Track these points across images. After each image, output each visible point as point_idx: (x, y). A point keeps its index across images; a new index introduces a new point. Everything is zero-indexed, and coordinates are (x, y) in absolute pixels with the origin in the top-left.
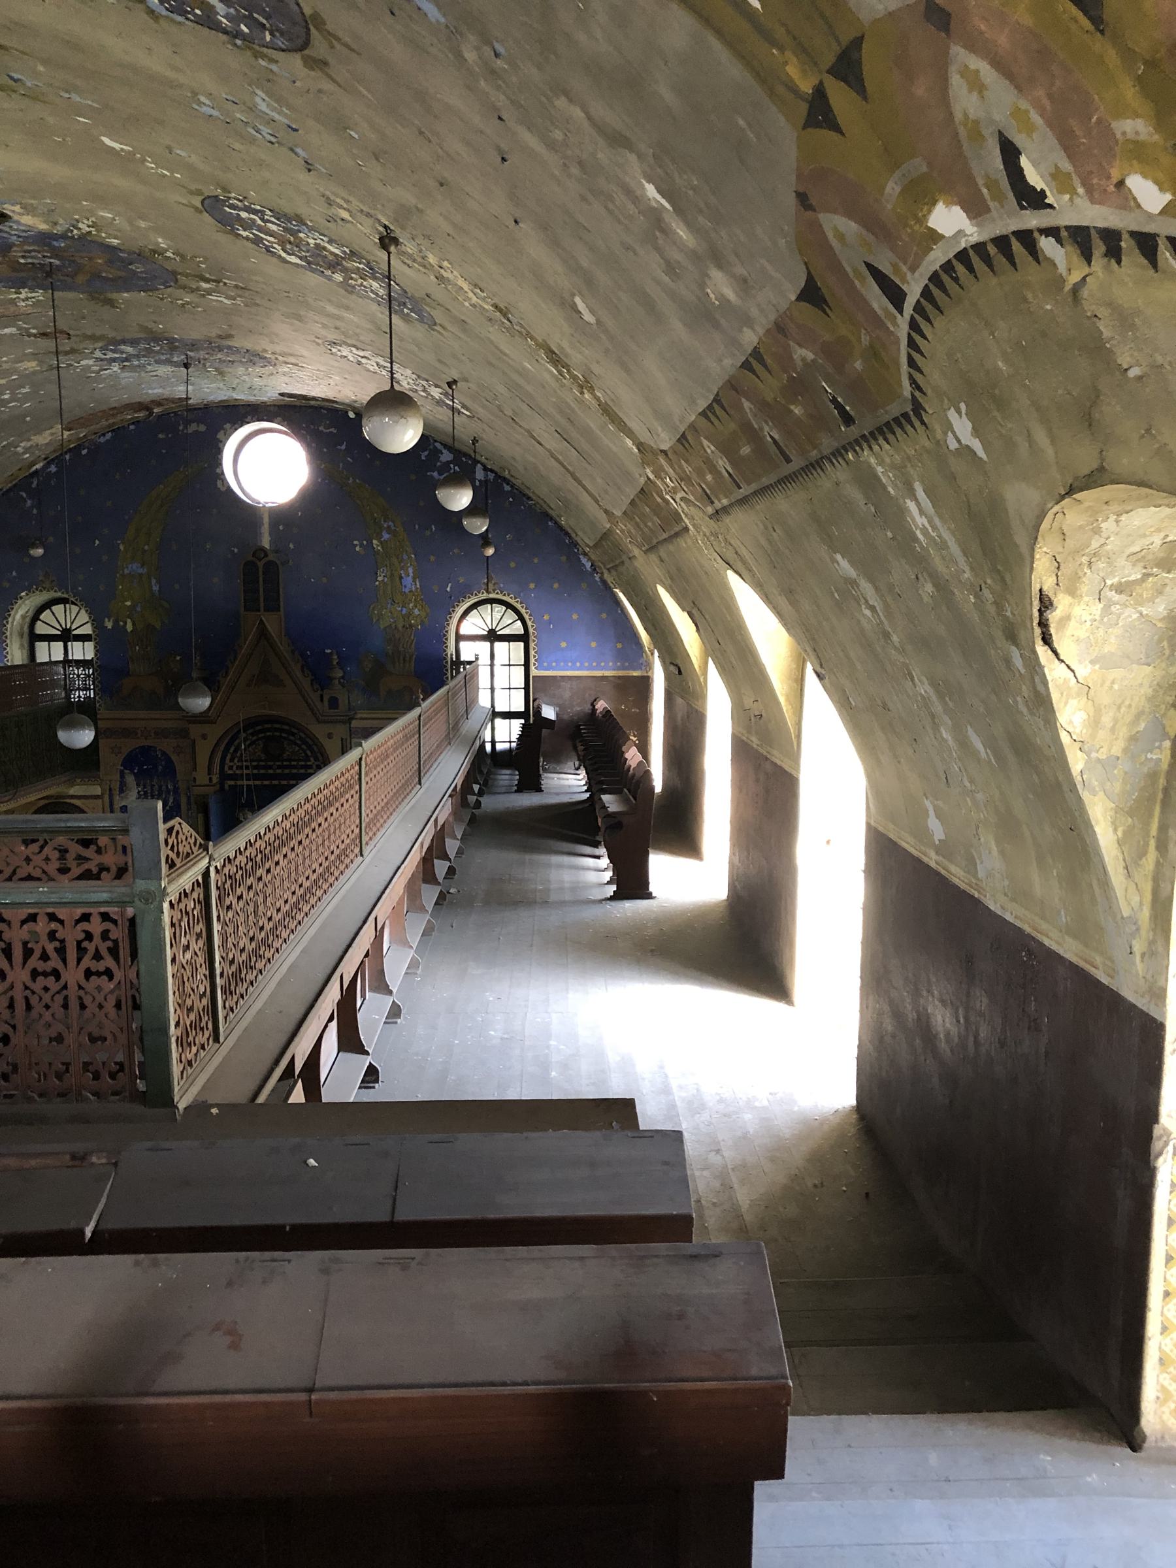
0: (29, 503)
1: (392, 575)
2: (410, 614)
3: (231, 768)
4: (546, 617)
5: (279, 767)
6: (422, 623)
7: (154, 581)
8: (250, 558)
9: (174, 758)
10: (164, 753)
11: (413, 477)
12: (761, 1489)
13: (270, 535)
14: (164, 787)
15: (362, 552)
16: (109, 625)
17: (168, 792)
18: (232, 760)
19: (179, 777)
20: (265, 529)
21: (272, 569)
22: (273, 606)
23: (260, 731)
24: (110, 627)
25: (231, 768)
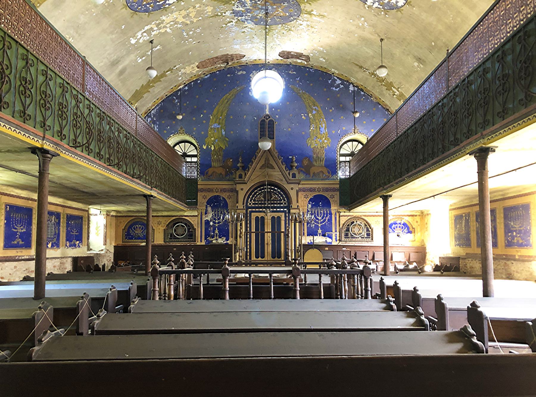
7: (223, 130)
10: (223, 198)
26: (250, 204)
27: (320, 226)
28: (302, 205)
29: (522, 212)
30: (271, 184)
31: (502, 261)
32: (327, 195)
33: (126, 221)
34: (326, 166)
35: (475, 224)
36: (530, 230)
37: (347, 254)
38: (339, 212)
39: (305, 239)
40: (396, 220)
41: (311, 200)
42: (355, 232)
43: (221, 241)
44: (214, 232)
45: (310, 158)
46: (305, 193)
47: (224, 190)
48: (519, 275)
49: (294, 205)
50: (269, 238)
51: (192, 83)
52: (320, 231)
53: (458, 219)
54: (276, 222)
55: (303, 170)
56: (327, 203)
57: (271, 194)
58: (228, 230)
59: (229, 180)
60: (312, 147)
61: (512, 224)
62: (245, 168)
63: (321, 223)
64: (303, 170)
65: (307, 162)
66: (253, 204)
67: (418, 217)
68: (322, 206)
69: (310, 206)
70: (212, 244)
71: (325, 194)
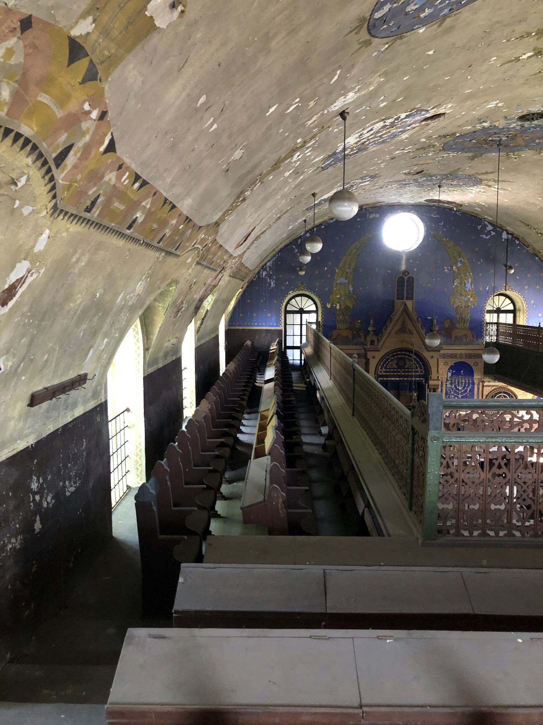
0: (296, 250)
1: (461, 283)
2: (469, 300)
3: (381, 372)
4: (532, 302)
5: (403, 372)
6: (474, 305)
7: (350, 286)
8: (401, 275)
11: (473, 237)
13: (406, 264)
15: (448, 272)
16: (329, 306)
18: (381, 368)
20: (403, 262)
21: (411, 281)
22: (410, 298)
24: (329, 307)
25: (381, 372)
34: (471, 329)
38: (483, 382)
41: (451, 368)
46: (444, 360)
49: (434, 375)
51: (315, 229)
62: (378, 332)
63: (462, 393)
66: (384, 372)
68: (464, 375)
69: (450, 374)
71: (468, 361)
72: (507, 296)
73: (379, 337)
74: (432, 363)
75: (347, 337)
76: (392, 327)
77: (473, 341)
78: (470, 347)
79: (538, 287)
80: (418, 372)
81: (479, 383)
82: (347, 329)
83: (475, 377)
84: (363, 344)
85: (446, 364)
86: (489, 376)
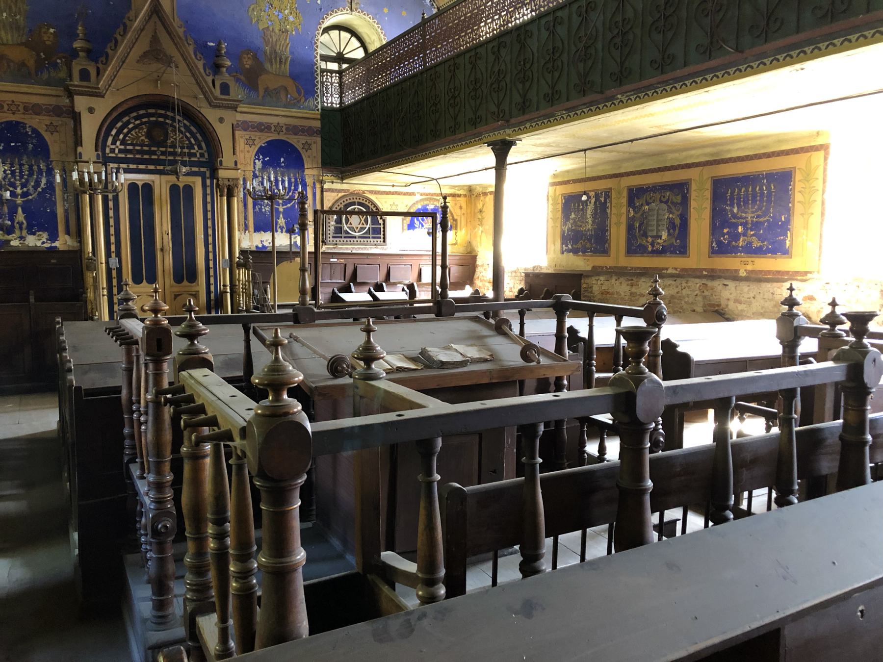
2: (286, 19)
5: (163, 153)
9: (47, 136)
10: (35, 131)
12: (679, 349)
14: (35, 168)
17: (40, 172)
18: (114, 143)
19: (53, 157)
23: (143, 116)
25: (112, 151)
26: (112, 151)
27: (281, 210)
28: (242, 161)
29: (769, 188)
30: (164, 103)
31: (697, 280)
32: (297, 141)
33: (151, 183)
34: (294, 77)
35: (624, 210)
36: (788, 222)
37: (339, 270)
38: (322, 182)
39: (251, 239)
40: (426, 203)
41: (261, 151)
42: (354, 225)
43: (34, 241)
44: (12, 219)
45: (256, 54)
46: (247, 134)
47: (36, 109)
48: (741, 307)
49: (227, 158)
50: (165, 237)
52: (282, 221)
53: (570, 204)
54: (181, 198)
55: (242, 78)
56: (296, 161)
57: (165, 130)
58: (54, 215)
59: (47, 83)
60: (261, 27)
61: (735, 210)
62: (98, 54)
64: (242, 78)
65: (250, 62)
66: (120, 151)
67: (462, 199)
68: (287, 167)
69: (259, 164)
70: (9, 249)
71: (293, 140)
72: (354, 33)
73: (100, 65)
74: (223, 132)
75: (23, 64)
76: (130, 47)
77: (299, 102)
78: (294, 112)
79: (404, 13)
80: (194, 155)
81: (314, 184)
82: (22, 44)
83: (307, 172)
84: (60, 83)
85: (250, 142)
86: (331, 172)
